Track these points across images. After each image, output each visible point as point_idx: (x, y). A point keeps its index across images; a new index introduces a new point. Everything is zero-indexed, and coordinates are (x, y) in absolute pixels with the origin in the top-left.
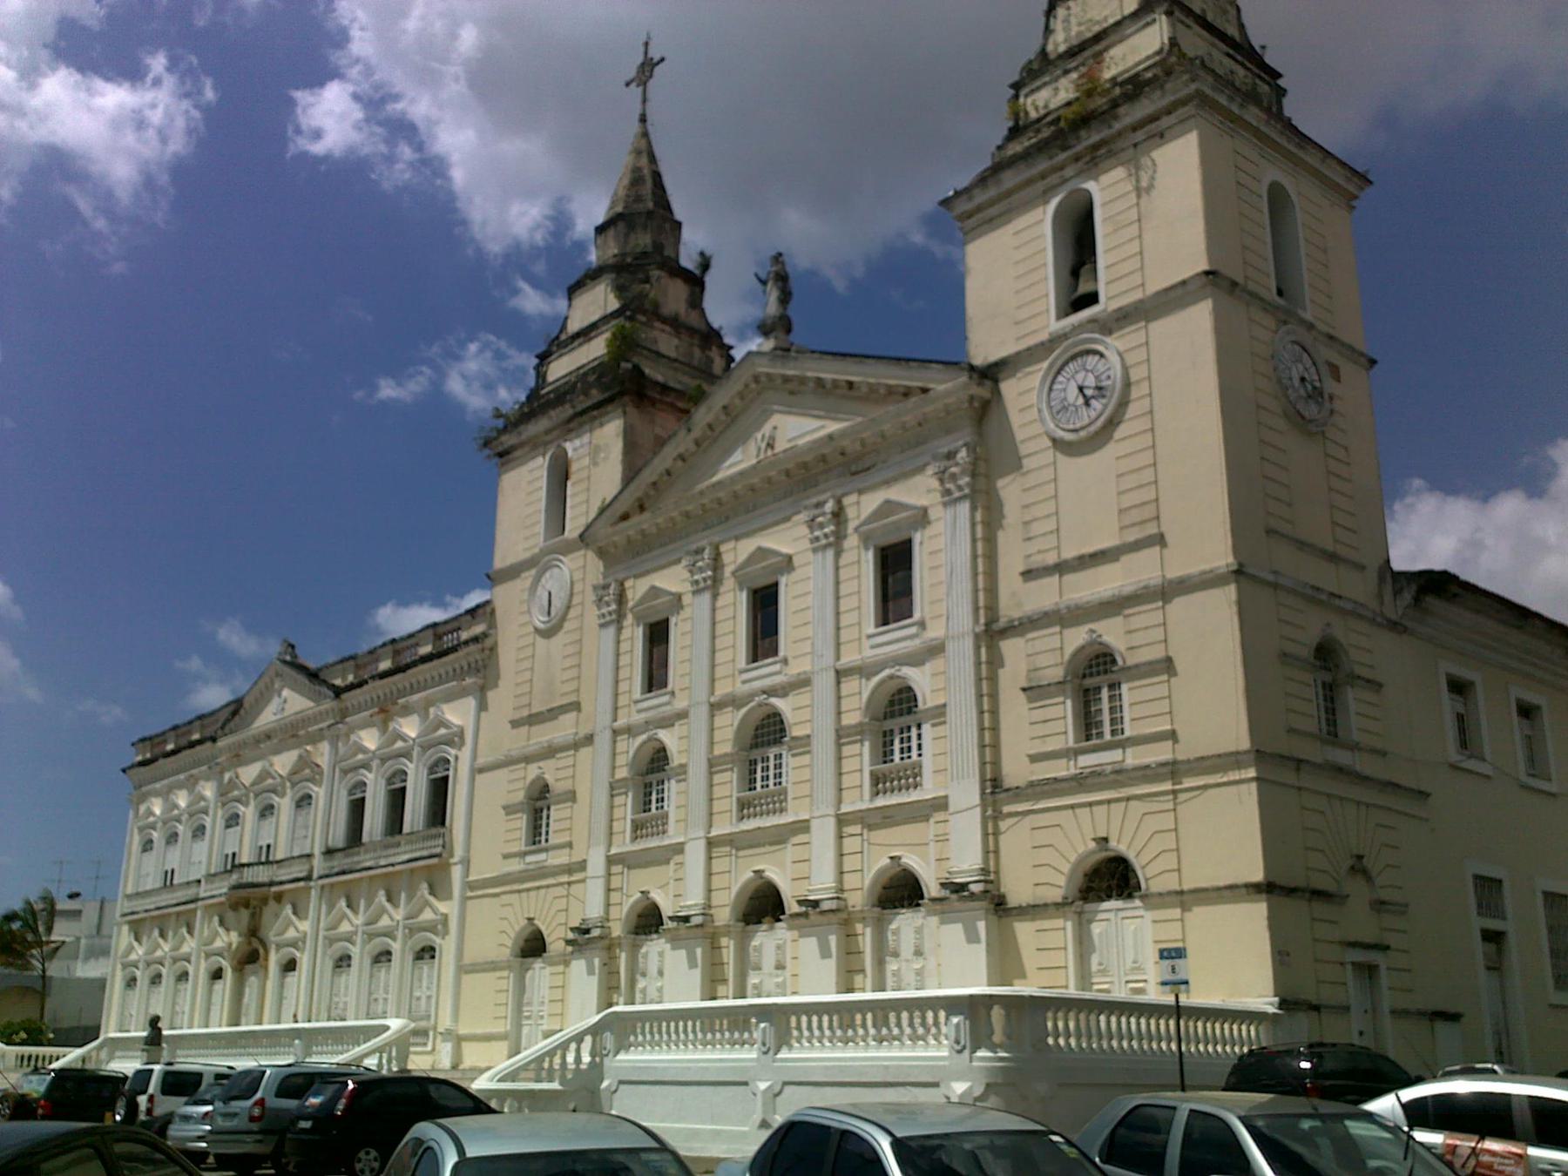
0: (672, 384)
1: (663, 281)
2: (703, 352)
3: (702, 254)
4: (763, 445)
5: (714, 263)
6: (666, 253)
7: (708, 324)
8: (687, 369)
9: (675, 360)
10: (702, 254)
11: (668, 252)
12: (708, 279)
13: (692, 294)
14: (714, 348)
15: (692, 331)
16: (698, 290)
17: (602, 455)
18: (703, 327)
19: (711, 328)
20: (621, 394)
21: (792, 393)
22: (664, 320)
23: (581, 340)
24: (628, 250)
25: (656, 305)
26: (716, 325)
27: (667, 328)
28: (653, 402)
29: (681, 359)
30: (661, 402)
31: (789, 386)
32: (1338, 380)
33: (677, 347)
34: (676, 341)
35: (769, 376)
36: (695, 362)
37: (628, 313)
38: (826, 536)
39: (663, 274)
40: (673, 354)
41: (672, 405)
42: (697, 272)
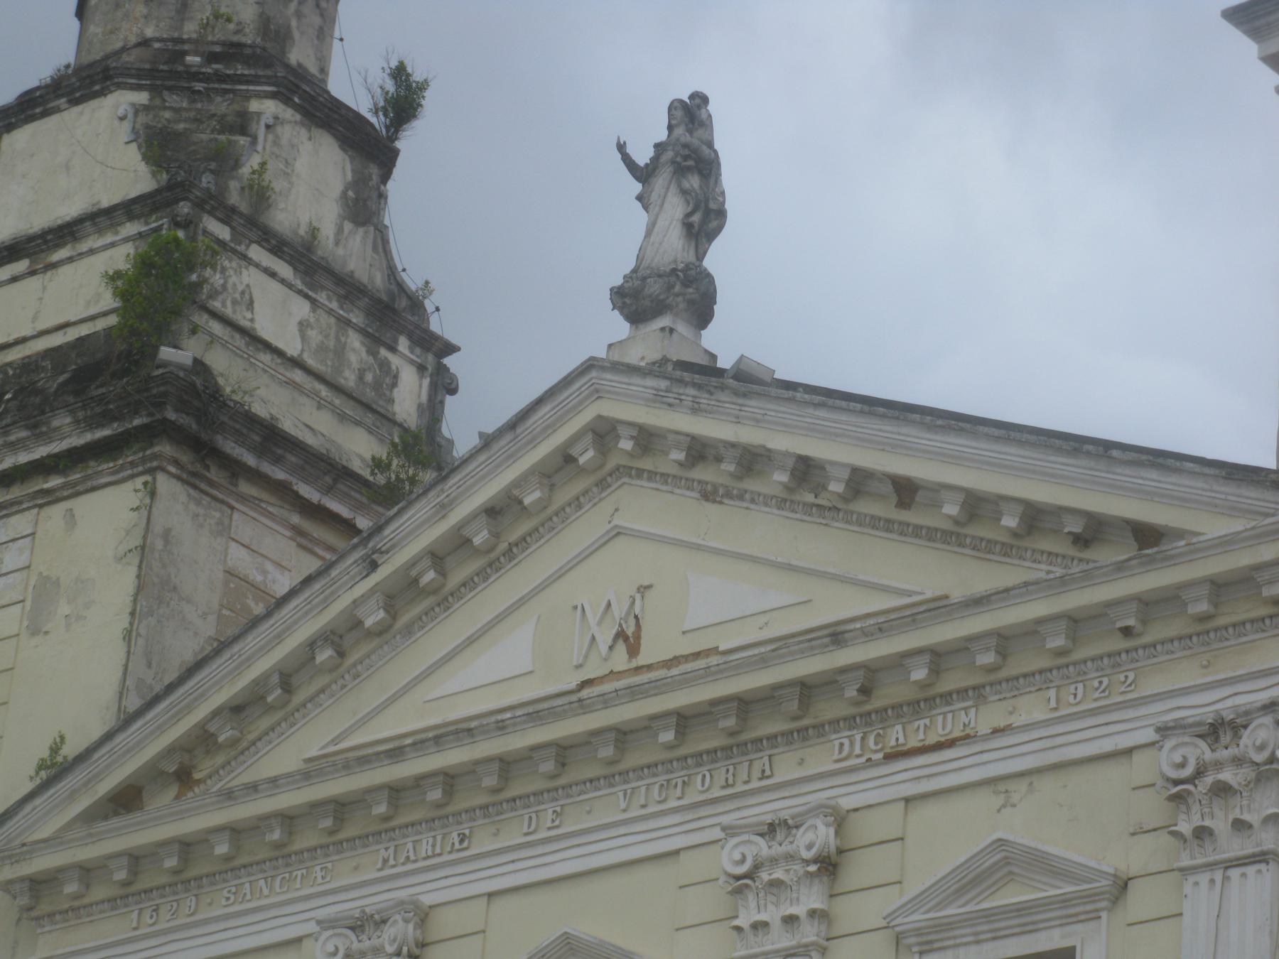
0: (287, 425)
1: (286, 132)
2: (373, 353)
3: (400, 73)
4: (605, 637)
5: (430, 101)
6: (294, 57)
7: (392, 272)
8: (324, 391)
9: (296, 363)
10: (400, 73)
11: (300, 54)
12: (410, 143)
13: (359, 182)
14: (403, 344)
15: (349, 289)
16: (374, 171)
17: (64, 609)
18: (378, 281)
19: (401, 286)
20: (148, 434)
21: (709, 495)
22: (278, 246)
23: (22, 266)
24: (190, 29)
25: (261, 195)
26: (413, 281)
27: (285, 270)
28: (235, 469)
29: (310, 361)
30: (257, 477)
31: (704, 473)
32: (62, 738)
33: (303, 326)
34: (301, 308)
35: (647, 439)
36: (349, 379)
37: (184, 208)
38: (790, 920)
39: (288, 113)
40: (292, 347)
41: (283, 491)
42: (377, 121)
